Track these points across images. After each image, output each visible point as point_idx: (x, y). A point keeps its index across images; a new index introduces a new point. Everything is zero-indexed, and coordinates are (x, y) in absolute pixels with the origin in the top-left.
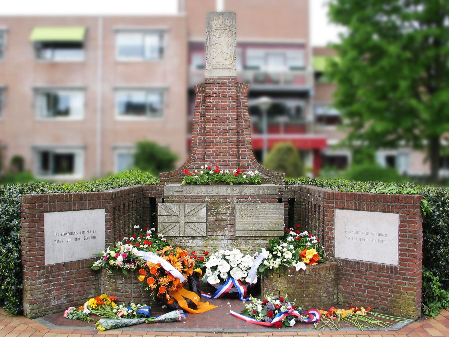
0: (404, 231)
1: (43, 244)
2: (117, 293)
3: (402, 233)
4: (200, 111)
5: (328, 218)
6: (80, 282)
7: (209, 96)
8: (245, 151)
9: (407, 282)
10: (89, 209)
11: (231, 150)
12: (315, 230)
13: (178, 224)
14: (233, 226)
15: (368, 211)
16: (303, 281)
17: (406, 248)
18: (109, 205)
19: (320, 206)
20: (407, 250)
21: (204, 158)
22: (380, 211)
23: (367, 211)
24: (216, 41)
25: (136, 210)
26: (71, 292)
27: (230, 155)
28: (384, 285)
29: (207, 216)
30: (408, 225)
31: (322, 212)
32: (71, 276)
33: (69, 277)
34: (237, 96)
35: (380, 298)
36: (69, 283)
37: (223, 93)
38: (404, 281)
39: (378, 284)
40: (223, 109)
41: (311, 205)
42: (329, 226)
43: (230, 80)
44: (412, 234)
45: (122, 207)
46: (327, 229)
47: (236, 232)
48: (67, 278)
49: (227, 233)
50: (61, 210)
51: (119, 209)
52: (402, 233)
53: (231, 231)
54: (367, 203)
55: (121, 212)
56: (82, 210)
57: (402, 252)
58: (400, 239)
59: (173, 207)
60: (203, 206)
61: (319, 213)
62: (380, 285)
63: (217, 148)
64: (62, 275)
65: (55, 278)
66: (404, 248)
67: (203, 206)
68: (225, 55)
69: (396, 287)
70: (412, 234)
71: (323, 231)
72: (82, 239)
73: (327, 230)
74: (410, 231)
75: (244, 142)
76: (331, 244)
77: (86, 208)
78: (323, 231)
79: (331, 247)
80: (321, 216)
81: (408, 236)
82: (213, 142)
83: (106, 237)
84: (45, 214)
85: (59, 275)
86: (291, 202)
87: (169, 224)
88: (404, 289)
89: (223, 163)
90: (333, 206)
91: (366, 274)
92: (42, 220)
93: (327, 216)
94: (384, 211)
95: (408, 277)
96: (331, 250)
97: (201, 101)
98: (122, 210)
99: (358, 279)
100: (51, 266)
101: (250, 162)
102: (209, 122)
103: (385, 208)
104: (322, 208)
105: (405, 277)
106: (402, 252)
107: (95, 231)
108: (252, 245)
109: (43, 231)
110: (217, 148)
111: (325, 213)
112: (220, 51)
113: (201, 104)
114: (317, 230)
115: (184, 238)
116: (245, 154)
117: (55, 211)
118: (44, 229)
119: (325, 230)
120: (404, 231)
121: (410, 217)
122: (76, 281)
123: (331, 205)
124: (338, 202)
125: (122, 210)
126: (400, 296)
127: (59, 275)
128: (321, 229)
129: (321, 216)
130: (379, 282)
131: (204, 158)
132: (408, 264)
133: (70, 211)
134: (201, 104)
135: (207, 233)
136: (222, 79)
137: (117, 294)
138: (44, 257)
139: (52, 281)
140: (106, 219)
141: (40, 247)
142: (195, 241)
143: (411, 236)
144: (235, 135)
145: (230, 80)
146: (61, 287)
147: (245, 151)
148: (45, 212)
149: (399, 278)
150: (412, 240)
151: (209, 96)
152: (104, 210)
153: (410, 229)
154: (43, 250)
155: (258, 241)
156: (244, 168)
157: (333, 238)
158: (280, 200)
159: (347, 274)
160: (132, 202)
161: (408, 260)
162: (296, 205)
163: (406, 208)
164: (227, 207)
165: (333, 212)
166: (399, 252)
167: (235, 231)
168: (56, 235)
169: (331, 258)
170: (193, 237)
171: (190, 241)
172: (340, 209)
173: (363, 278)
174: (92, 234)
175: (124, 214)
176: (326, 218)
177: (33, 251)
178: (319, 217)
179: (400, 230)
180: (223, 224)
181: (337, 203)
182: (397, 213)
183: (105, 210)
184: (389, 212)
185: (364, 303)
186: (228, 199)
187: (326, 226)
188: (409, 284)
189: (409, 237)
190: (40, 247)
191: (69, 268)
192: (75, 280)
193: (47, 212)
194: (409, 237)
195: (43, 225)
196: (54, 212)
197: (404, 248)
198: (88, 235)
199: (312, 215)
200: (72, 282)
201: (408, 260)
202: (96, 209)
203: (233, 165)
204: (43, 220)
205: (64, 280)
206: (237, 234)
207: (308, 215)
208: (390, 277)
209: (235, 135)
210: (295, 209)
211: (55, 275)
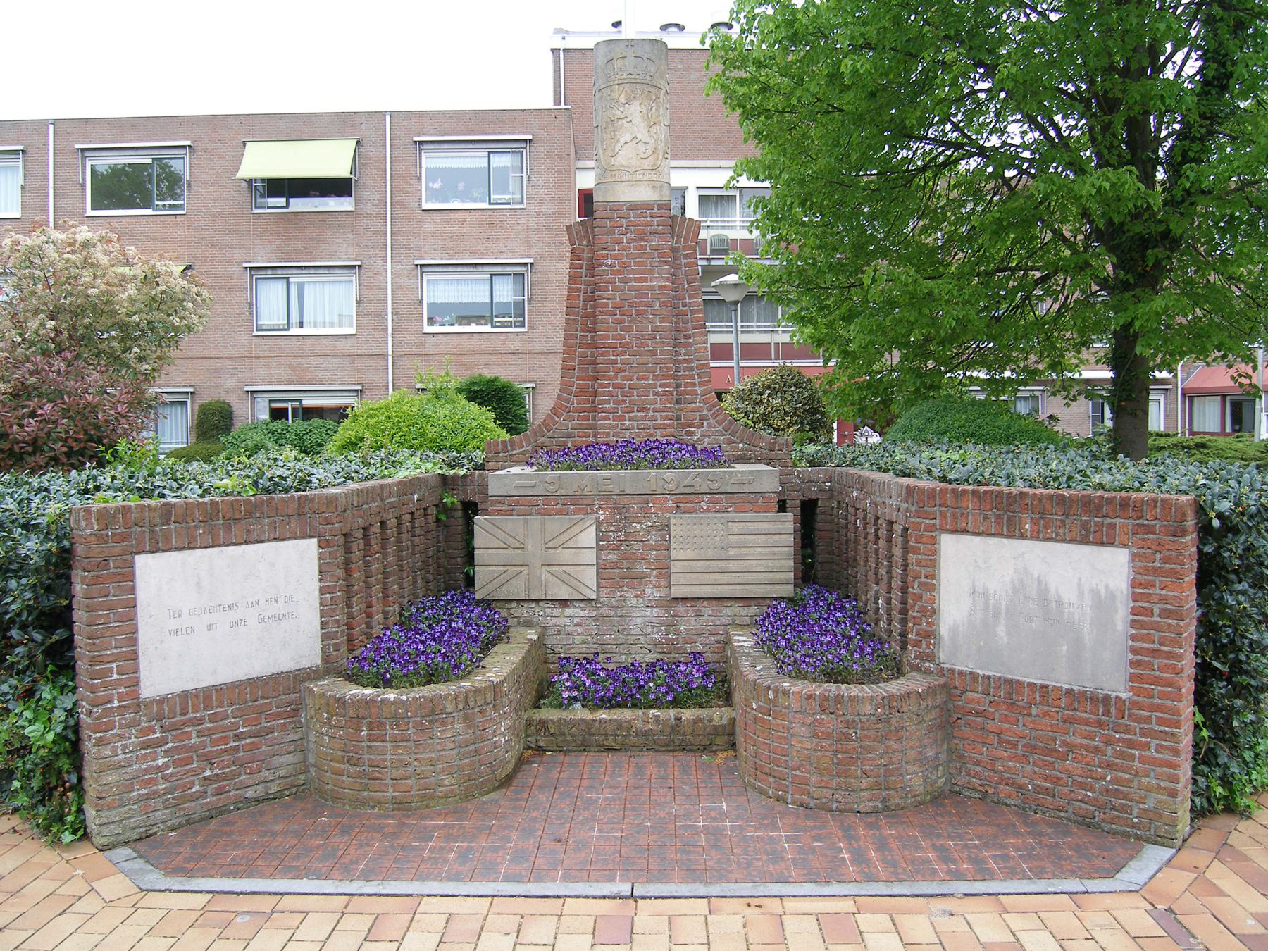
0: (1147, 597)
1: (134, 641)
2: (346, 766)
3: (1140, 604)
4: (583, 287)
5: (920, 557)
6: (250, 737)
7: (604, 249)
8: (691, 369)
9: (1154, 743)
10: (269, 541)
11: (658, 383)
12: (877, 584)
13: (525, 570)
14: (664, 571)
15: (1037, 538)
16: (856, 733)
17: (1152, 646)
18: (329, 526)
19: (891, 523)
20: (1153, 653)
21: (593, 402)
22: (1072, 541)
23: (1032, 538)
24: (619, 113)
25: (423, 533)
26: (223, 768)
27: (657, 394)
28: (1082, 746)
29: (599, 548)
30: (1157, 582)
31: (900, 539)
32: (221, 723)
33: (215, 728)
34: (674, 250)
35: (1070, 780)
36: (214, 743)
37: (636, 241)
38: (1143, 739)
39: (1064, 743)
40: (636, 280)
41: (865, 518)
42: (923, 579)
43: (655, 210)
44: (1169, 607)
45: (376, 529)
46: (916, 587)
47: (673, 588)
48: (209, 729)
49: (648, 591)
50: (191, 545)
51: (366, 537)
52: (1140, 604)
53: (659, 586)
54: (1032, 519)
55: (373, 542)
56: (251, 542)
57: (1140, 657)
58: (1133, 621)
59: (513, 524)
60: (588, 523)
61: (889, 540)
62: (1071, 747)
63: (624, 378)
64: (192, 722)
65: (174, 733)
66: (1145, 645)
67: (588, 523)
68: (642, 147)
69: (1121, 755)
70: (1169, 607)
71: (904, 590)
72: (252, 622)
73: (915, 589)
74: (1163, 600)
75: (691, 361)
76: (930, 629)
77: (262, 538)
78: (904, 590)
79: (929, 636)
80: (897, 551)
81: (1156, 611)
82: (614, 362)
83: (323, 614)
84: (137, 557)
85: (185, 724)
86: (808, 510)
87: (505, 569)
88: (1143, 760)
89: (639, 414)
90: (934, 525)
91: (1030, 715)
92: (127, 575)
93: (916, 551)
94: (1085, 541)
95: (1157, 728)
96: (928, 644)
97: (585, 263)
98: (375, 540)
99: (1006, 726)
100: (162, 701)
101: (705, 412)
102: (604, 313)
103: (1088, 531)
104: (898, 528)
105: (1146, 726)
106: (1140, 657)
107: (288, 600)
108: (712, 621)
109: (132, 604)
110: (624, 378)
111: (911, 543)
112: (628, 137)
113: (583, 271)
114: (884, 584)
115: (541, 603)
116: (694, 393)
117: (169, 550)
118: (135, 599)
119: (911, 589)
120: (1147, 597)
121: (1166, 560)
122: (236, 736)
123: (927, 521)
124: (949, 515)
125: (375, 540)
126: (1132, 781)
127: (185, 724)
128: (896, 584)
129: (897, 551)
130: (1070, 738)
131: (593, 402)
132: (1156, 692)
133: (213, 546)
134: (583, 271)
135: (598, 592)
136: (634, 206)
137: (348, 771)
138: (138, 678)
139: (162, 742)
140: (320, 565)
141: (124, 650)
142: (568, 611)
143: (1166, 614)
144: (668, 344)
145: (655, 210)
146: (192, 757)
147: (694, 385)
148: (139, 553)
149: (1127, 730)
150: (1169, 625)
151: (604, 249)
152: (314, 541)
153: (1164, 592)
154: (134, 657)
155: (729, 611)
156: (691, 425)
157: (934, 612)
158: (782, 507)
159: (974, 709)
160: (412, 513)
161: (1157, 681)
162: (819, 518)
163: (1154, 533)
164: (650, 524)
165: (934, 541)
166: (1130, 656)
167: (669, 586)
168: (175, 614)
169: (927, 664)
170: (564, 603)
171: (556, 612)
172: (955, 531)
173: (1020, 724)
174: (281, 607)
175: (384, 548)
176: (912, 558)
177: (102, 663)
178: (889, 550)
179: (1133, 593)
180: (641, 568)
181: (945, 517)
182: (1125, 546)
183: (319, 542)
184: (1102, 544)
185: (1023, 792)
186: (651, 505)
187: (915, 578)
188: (1159, 749)
189: (1159, 616)
190: (124, 650)
191: (215, 704)
192: (231, 734)
193: (143, 552)
194: (1159, 616)
195: (132, 590)
196: (164, 551)
197: (1145, 645)
198: (272, 610)
199: (866, 544)
200: (225, 740)
201: (1157, 681)
202: (290, 539)
203: (663, 418)
204: (131, 576)
205: (198, 737)
206: (677, 592)
207: (856, 542)
208: (1099, 723)
209: (668, 344)
210: (818, 526)
211: (175, 724)
